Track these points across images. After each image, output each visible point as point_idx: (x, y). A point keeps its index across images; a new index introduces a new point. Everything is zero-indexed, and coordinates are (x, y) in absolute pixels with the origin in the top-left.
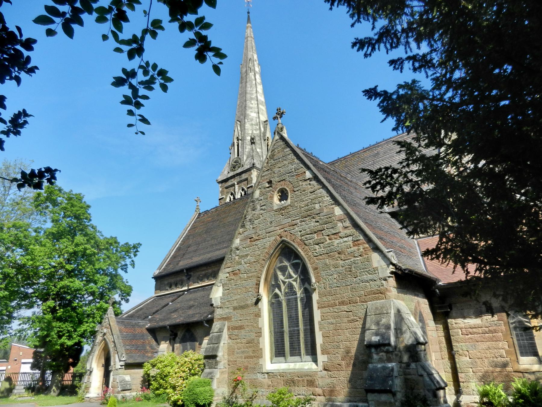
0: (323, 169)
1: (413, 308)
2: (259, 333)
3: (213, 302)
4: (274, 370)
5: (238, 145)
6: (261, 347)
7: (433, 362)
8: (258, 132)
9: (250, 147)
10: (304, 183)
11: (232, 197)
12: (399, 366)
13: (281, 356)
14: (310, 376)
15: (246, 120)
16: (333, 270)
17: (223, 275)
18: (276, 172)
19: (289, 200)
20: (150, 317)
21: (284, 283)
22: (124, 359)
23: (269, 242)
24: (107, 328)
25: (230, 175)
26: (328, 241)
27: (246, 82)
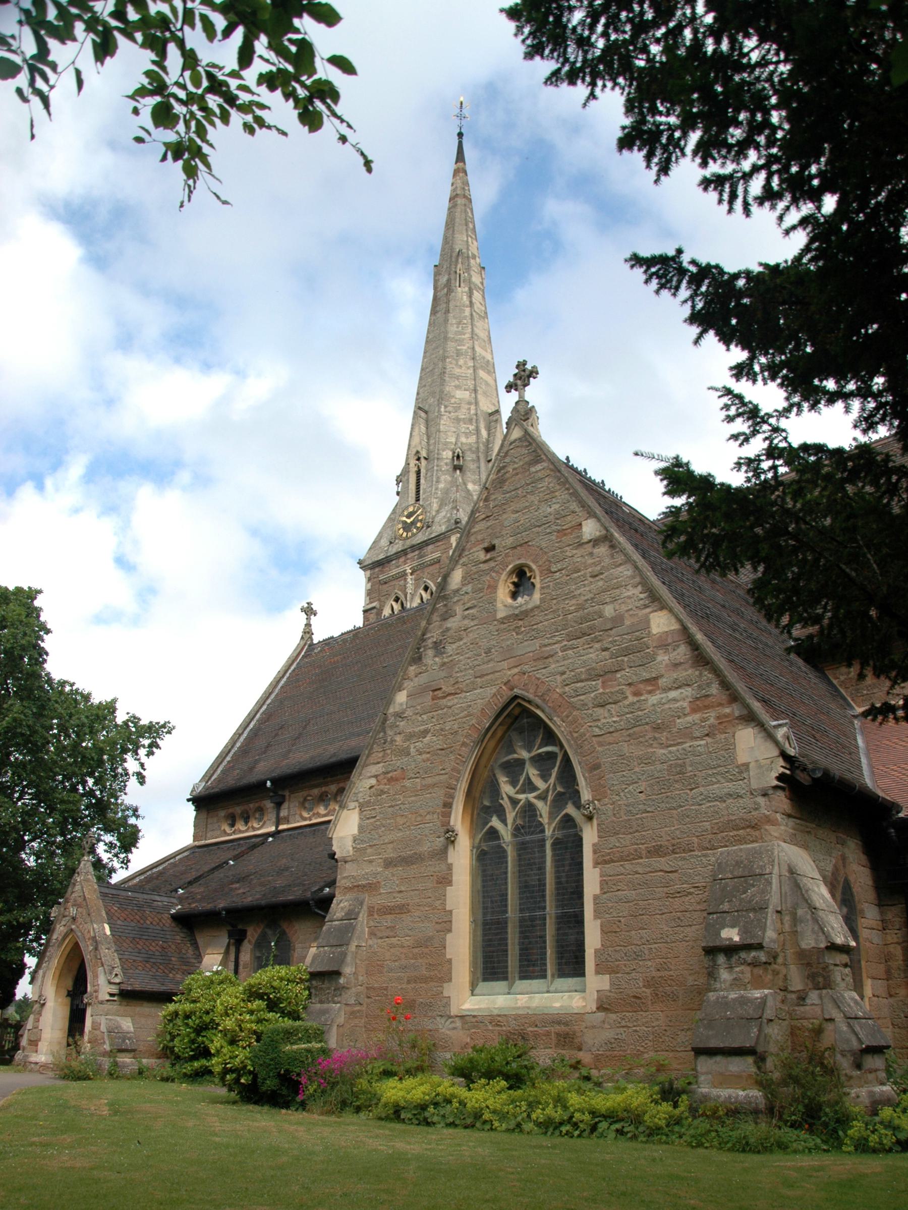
0: (630, 524)
1: (830, 868)
2: (446, 925)
3: (334, 848)
4: (479, 1010)
5: (418, 473)
6: (448, 957)
7: (866, 1000)
8: (472, 439)
9: (449, 478)
10: (579, 552)
11: (397, 607)
12: (779, 998)
13: (498, 979)
14: (566, 1024)
15: (442, 409)
16: (637, 769)
17: (363, 782)
18: (506, 523)
19: (537, 596)
20: (181, 891)
21: (514, 802)
22: (117, 980)
23: (479, 701)
24: (79, 906)
26: (631, 699)
27: (447, 311)
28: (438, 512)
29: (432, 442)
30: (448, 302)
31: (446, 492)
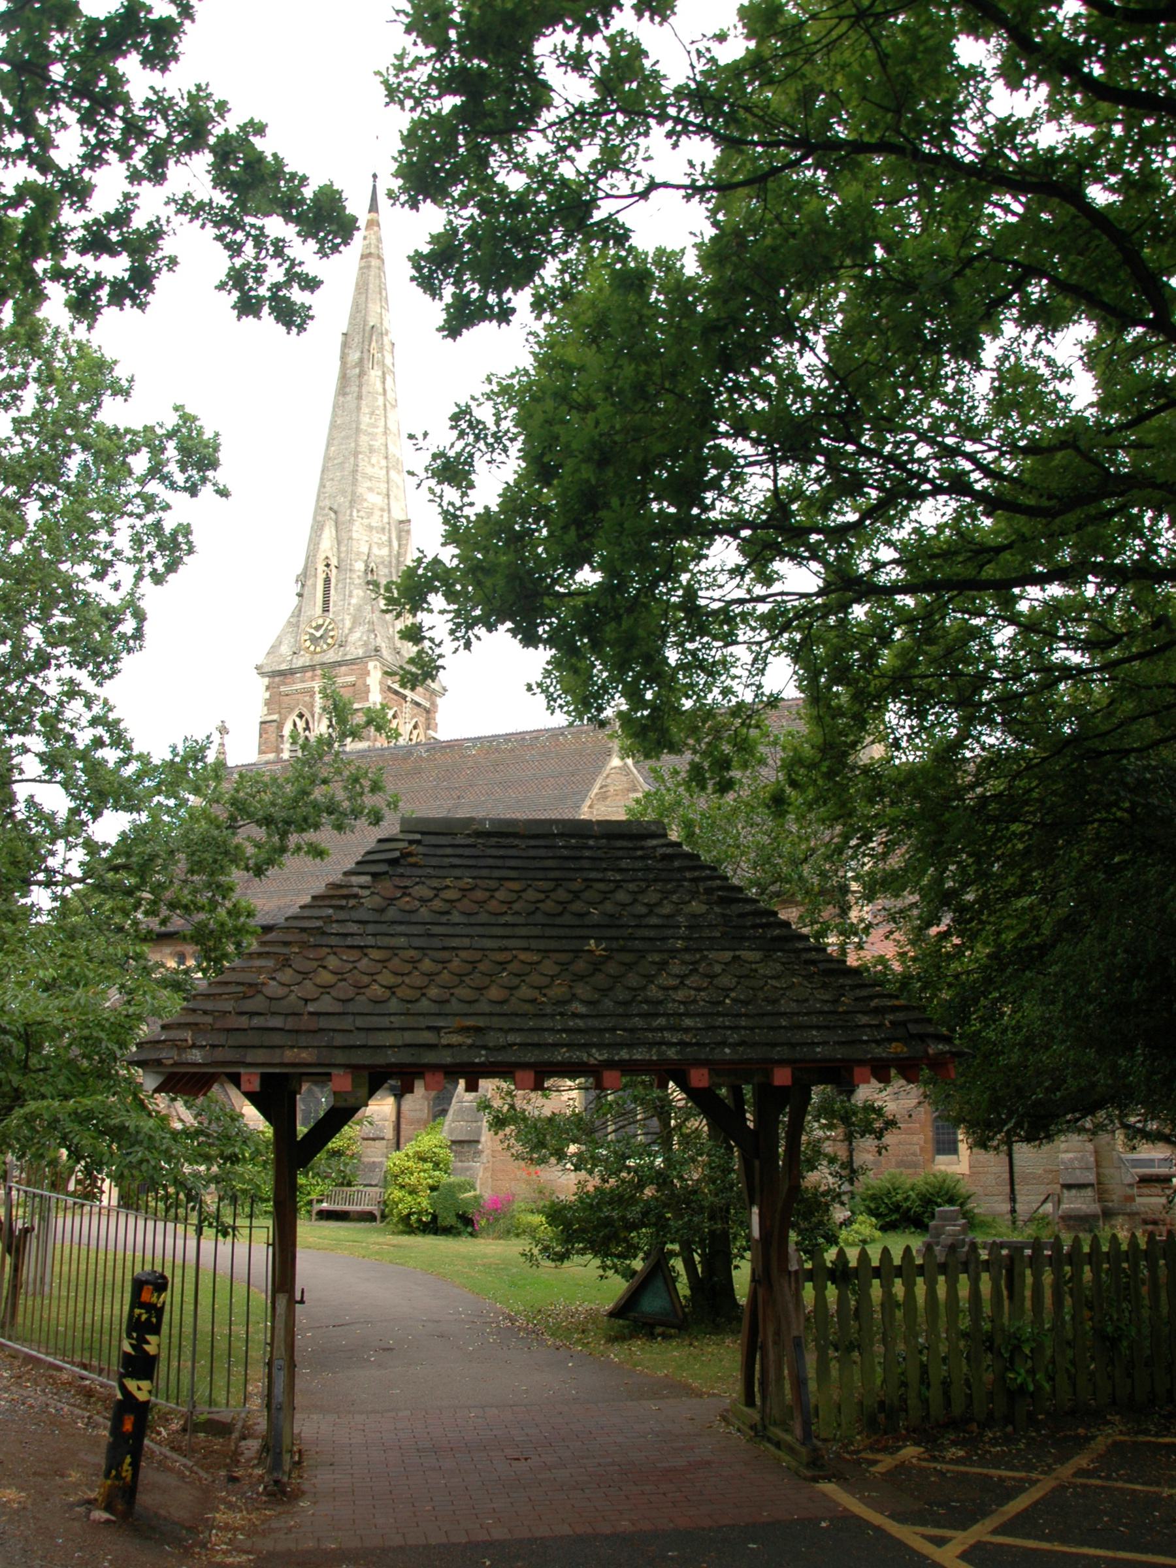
5: (327, 580)
8: (385, 551)
11: (301, 724)
25: (299, 662)
27: (359, 397)
28: (351, 630)
29: (343, 549)
30: (360, 386)
31: (359, 609)
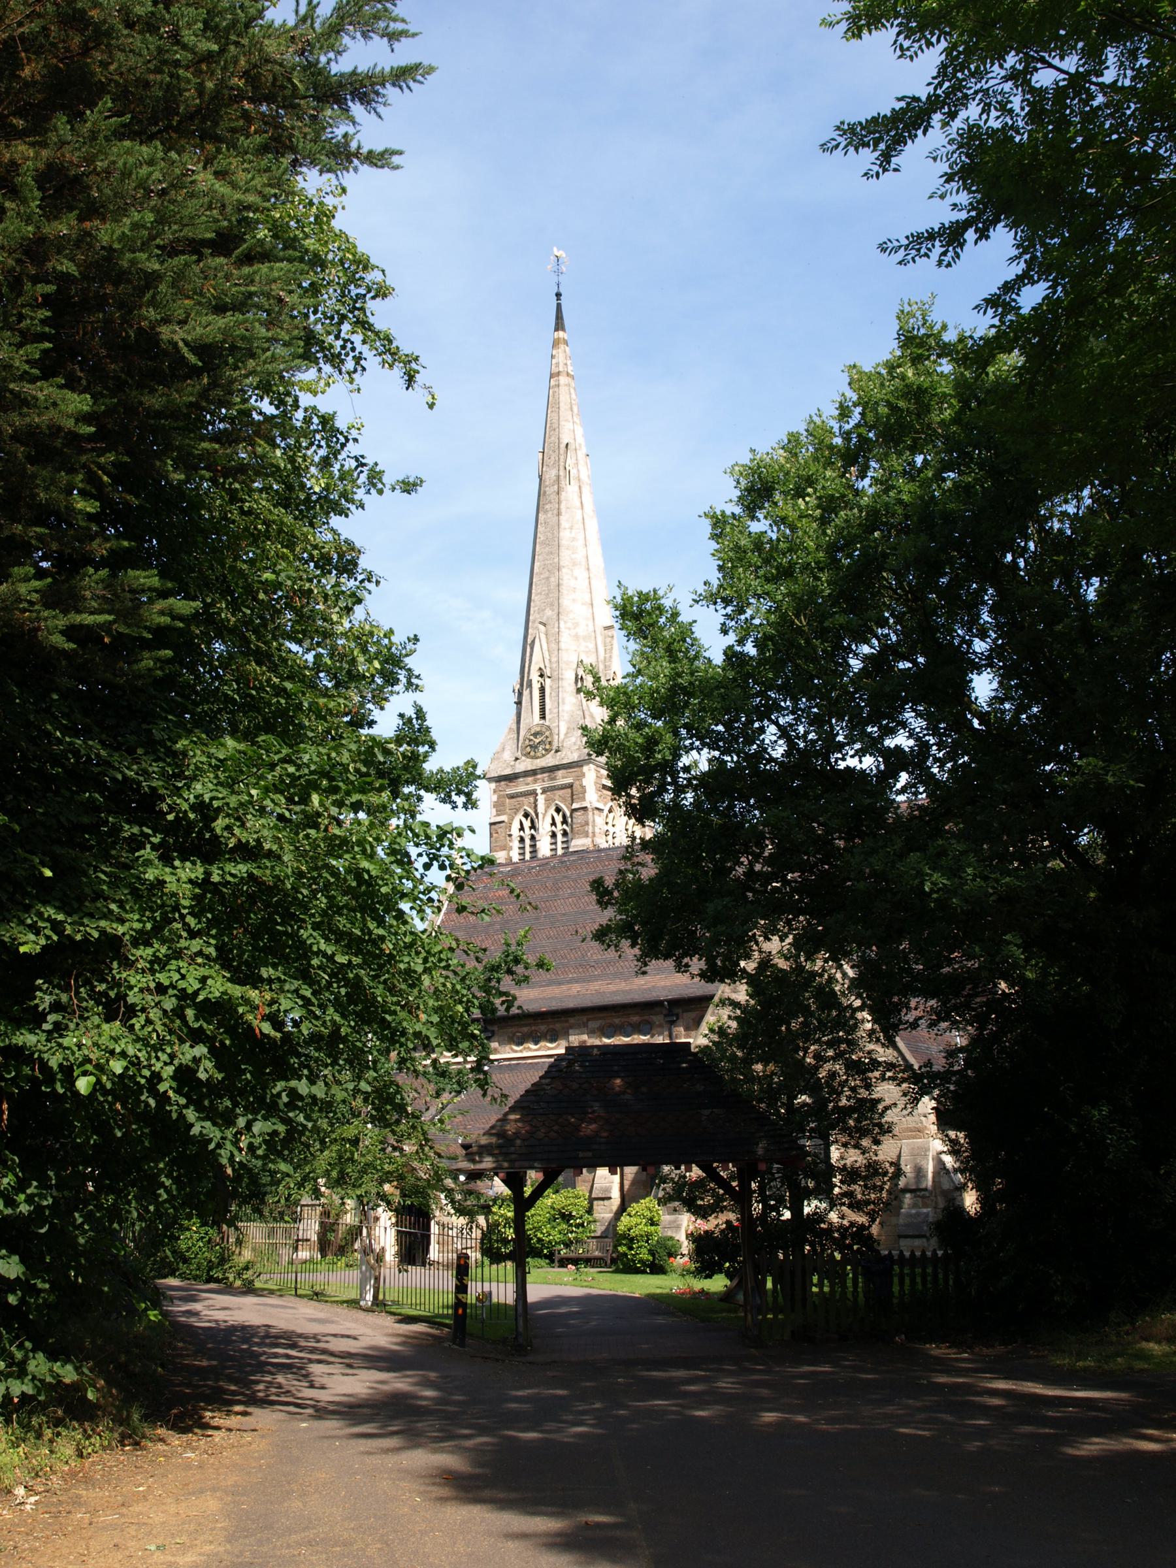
11: (527, 824)
25: (521, 767)
